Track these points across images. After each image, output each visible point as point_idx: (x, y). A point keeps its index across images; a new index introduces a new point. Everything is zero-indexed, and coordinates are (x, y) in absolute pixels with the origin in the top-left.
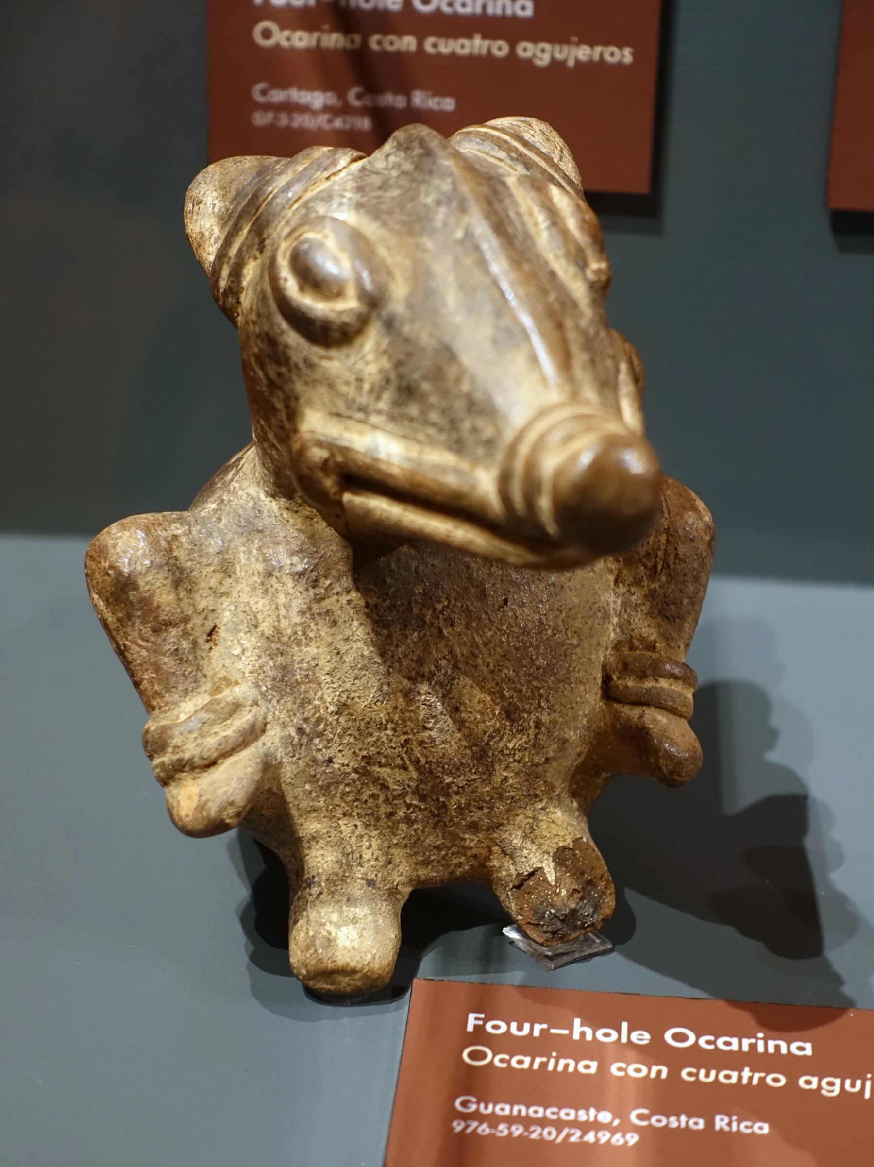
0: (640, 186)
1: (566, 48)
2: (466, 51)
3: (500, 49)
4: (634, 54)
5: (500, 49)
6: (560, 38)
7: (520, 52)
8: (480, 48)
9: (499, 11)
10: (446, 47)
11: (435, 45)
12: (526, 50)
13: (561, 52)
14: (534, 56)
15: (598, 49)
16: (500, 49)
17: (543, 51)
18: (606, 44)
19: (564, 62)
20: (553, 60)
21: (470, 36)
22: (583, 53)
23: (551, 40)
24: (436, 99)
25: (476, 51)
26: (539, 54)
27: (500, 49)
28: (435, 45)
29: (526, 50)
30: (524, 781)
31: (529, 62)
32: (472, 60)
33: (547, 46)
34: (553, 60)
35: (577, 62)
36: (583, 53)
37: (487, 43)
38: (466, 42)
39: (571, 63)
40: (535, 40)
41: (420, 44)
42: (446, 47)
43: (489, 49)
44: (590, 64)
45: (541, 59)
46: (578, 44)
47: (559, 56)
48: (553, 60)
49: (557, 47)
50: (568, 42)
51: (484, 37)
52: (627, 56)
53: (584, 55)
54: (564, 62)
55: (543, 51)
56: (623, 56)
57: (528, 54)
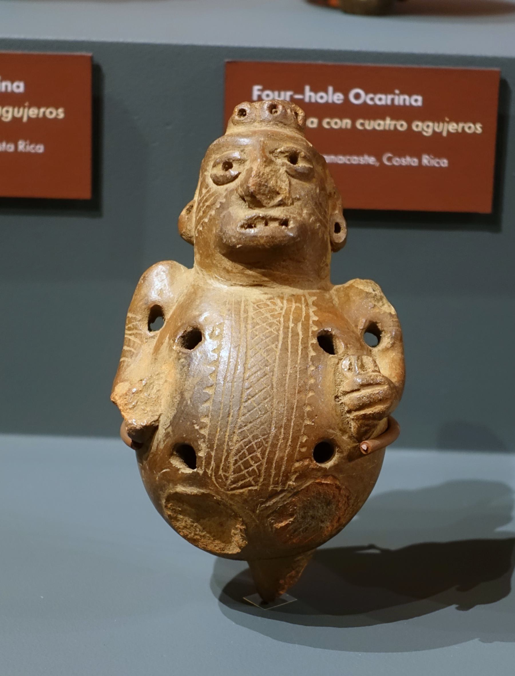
0: (86, 194)
1: (441, 124)
2: (381, 128)
3: (402, 125)
4: (65, 112)
5: (402, 126)
6: (438, 118)
7: (414, 128)
8: (390, 125)
9: (402, 103)
10: (370, 125)
11: (328, 123)
12: (418, 126)
13: (438, 127)
14: (423, 129)
15: (461, 125)
16: (402, 126)
17: (428, 126)
18: (465, 122)
19: (441, 133)
20: (14, 118)
21: (384, 119)
22: (453, 127)
23: (433, 121)
24: (32, 146)
25: (387, 128)
26: (425, 129)
27: (402, 125)
28: (362, 124)
29: (418, 126)
30: (183, 388)
31: (420, 133)
32: (384, 132)
33: (431, 124)
34: (14, 118)
35: (29, 118)
36: (453, 127)
37: (393, 122)
38: (382, 122)
39: (445, 134)
40: (423, 120)
41: (320, 123)
42: (370, 125)
43: (395, 126)
44: (37, 119)
45: (427, 132)
46: (29, 107)
47: (18, 115)
48: (434, 132)
49: (436, 124)
50: (443, 121)
51: (392, 119)
52: (478, 128)
53: (453, 129)
54: (441, 133)
55: (428, 126)
56: (476, 128)
57: (419, 129)
